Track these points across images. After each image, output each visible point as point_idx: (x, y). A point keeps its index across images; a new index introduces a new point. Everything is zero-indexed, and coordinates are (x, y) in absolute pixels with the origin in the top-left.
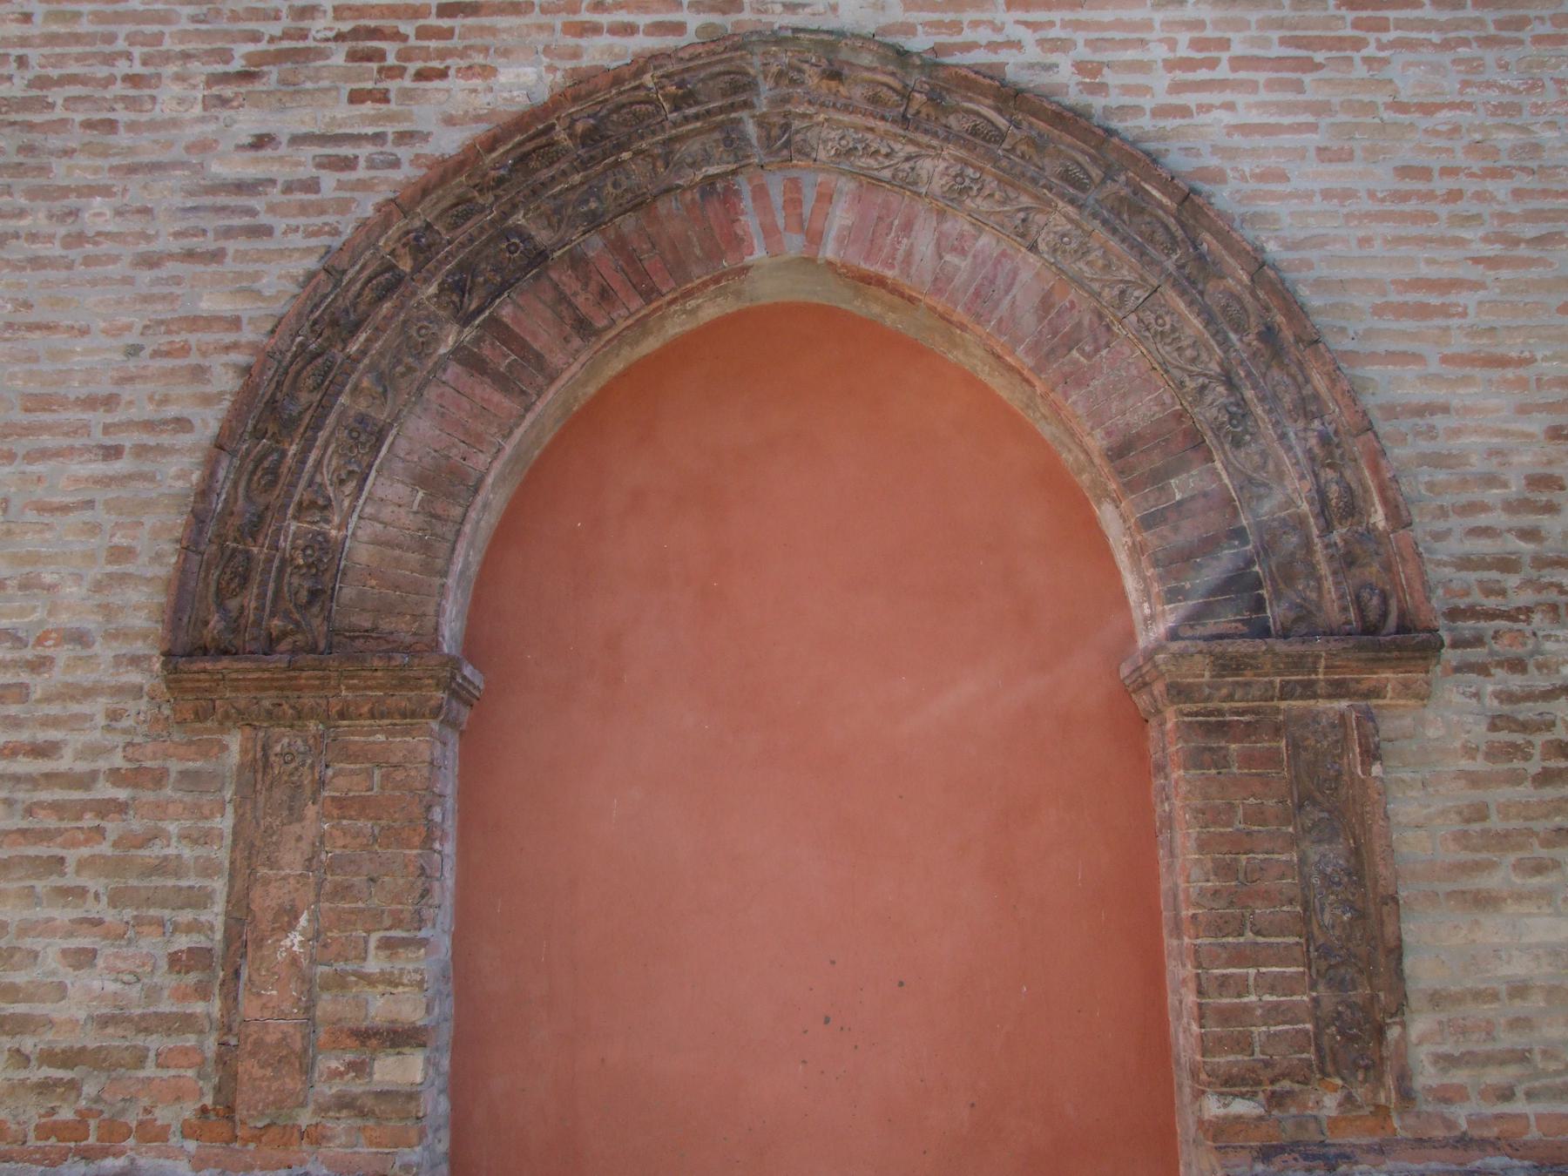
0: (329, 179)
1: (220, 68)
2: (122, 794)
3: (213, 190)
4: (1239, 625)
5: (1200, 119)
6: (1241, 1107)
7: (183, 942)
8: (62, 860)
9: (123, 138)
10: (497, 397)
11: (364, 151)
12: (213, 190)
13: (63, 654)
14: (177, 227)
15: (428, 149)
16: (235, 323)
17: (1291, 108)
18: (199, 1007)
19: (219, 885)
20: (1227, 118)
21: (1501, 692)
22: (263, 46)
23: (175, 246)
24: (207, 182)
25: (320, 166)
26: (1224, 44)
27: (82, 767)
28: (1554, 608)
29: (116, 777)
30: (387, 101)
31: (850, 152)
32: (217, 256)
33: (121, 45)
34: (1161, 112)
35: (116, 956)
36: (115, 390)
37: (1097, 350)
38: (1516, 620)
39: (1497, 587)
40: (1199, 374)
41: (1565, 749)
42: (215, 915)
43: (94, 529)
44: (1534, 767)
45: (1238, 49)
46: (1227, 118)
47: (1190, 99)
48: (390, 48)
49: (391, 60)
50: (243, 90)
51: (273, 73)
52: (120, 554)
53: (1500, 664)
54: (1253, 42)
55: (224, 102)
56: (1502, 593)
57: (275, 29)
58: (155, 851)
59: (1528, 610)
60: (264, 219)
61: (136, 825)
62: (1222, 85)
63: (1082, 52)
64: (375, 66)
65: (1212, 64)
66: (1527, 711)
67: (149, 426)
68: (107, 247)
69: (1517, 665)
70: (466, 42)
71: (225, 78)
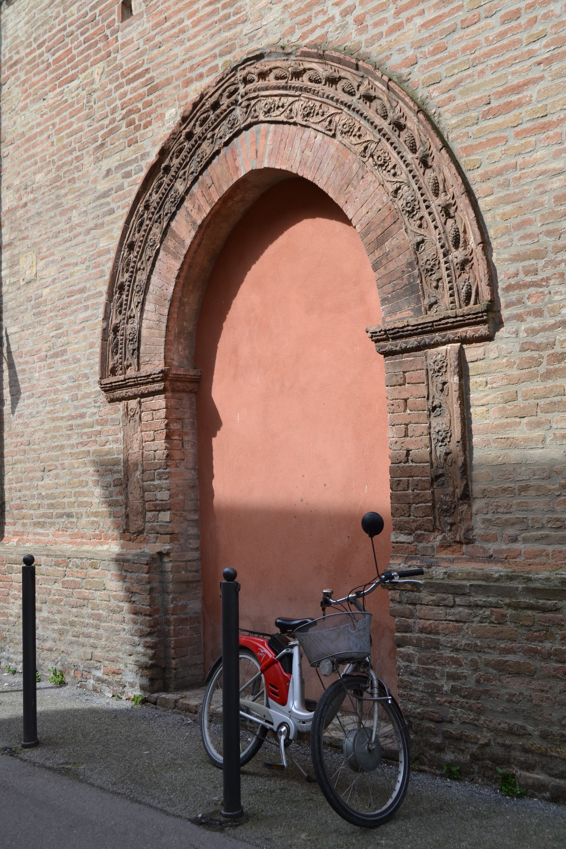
3: (98, 198)
4: (410, 312)
6: (402, 538)
12: (98, 198)
28: (562, 275)
29: (98, 423)
37: (359, 182)
38: (541, 286)
39: (532, 268)
40: (397, 182)
41: (560, 357)
44: (542, 369)
46: (419, 21)
53: (529, 314)
56: (536, 272)
57: (106, 122)
59: (548, 279)
61: (103, 438)
66: (539, 339)
69: (538, 313)
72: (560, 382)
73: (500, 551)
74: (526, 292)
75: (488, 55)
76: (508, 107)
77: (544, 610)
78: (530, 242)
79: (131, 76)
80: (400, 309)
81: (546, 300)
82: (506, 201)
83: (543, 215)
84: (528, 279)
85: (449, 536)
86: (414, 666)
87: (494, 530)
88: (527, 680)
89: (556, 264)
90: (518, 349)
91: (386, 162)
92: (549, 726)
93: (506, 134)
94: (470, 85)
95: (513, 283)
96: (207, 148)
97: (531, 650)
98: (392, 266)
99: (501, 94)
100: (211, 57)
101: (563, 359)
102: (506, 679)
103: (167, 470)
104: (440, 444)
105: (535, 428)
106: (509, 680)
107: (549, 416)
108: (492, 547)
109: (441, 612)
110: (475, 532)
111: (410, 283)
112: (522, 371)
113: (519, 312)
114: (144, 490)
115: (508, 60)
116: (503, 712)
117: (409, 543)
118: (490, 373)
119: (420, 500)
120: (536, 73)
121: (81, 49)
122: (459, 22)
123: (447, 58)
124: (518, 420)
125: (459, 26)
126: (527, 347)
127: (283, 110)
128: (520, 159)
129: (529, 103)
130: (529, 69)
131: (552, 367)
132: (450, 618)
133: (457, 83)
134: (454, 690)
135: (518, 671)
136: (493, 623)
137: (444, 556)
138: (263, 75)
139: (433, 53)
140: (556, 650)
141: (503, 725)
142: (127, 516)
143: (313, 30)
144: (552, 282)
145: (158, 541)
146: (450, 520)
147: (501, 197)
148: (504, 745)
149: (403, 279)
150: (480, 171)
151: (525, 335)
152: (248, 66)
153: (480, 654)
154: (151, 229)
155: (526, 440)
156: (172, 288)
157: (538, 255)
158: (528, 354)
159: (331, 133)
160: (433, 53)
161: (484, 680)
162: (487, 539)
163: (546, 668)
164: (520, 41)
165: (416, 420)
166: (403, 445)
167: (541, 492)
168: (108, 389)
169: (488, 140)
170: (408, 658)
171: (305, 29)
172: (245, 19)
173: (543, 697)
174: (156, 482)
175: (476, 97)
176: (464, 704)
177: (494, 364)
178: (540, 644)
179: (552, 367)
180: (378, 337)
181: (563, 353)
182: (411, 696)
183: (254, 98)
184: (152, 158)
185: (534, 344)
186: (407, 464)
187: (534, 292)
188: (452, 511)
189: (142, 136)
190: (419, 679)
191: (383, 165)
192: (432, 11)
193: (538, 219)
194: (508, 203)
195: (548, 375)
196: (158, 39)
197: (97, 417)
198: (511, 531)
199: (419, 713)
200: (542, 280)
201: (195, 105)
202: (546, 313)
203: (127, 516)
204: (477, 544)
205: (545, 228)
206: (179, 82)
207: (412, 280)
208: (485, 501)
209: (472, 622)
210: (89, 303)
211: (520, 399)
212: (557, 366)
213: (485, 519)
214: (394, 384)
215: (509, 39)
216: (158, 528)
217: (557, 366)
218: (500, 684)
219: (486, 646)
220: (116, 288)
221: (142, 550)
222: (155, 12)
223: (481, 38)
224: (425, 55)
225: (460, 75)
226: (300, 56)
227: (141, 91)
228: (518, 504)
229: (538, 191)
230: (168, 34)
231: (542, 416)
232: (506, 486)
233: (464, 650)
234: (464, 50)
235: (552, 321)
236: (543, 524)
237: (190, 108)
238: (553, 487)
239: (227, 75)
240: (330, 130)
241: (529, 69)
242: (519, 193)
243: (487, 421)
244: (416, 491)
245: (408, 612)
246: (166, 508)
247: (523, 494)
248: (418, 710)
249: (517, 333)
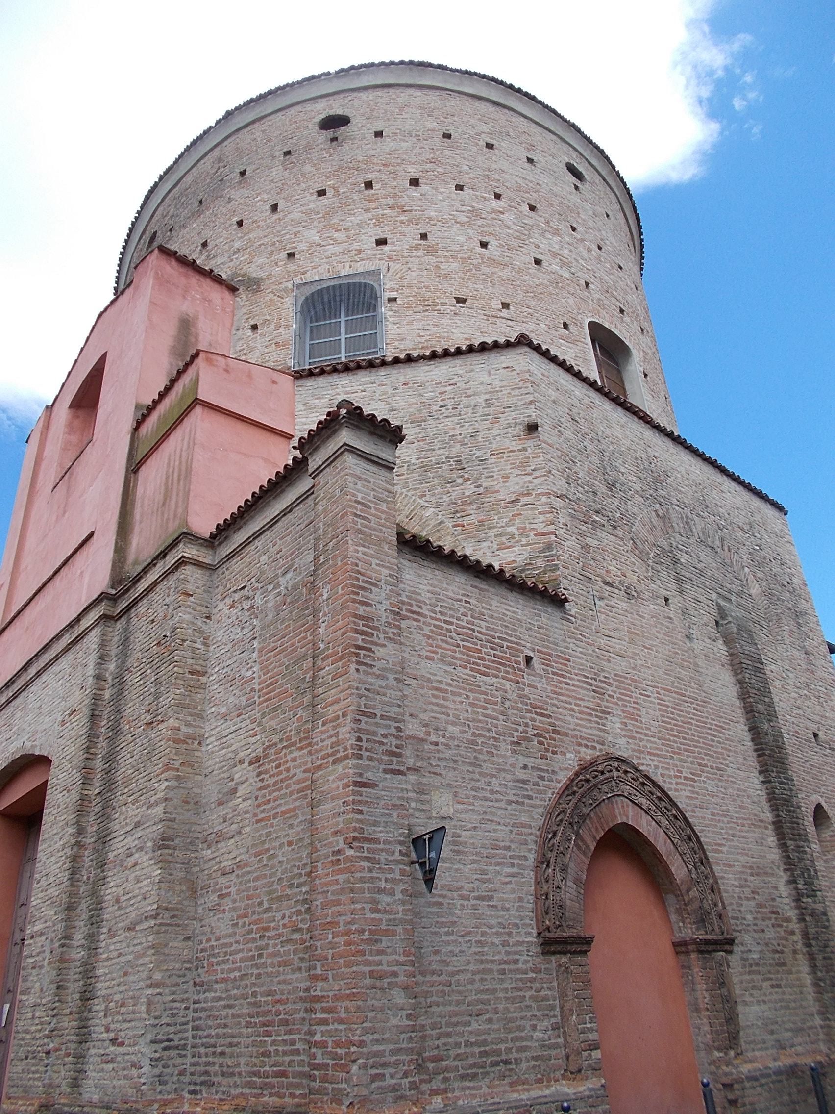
3: (519, 781)
12: (519, 781)
23: (514, 799)
27: (524, 967)
42: (557, 1012)
43: (513, 891)
58: (543, 993)
60: (530, 793)
68: (499, 796)
71: (513, 743)
142: (568, 1057)
196: (555, 702)
203: (568, 1057)
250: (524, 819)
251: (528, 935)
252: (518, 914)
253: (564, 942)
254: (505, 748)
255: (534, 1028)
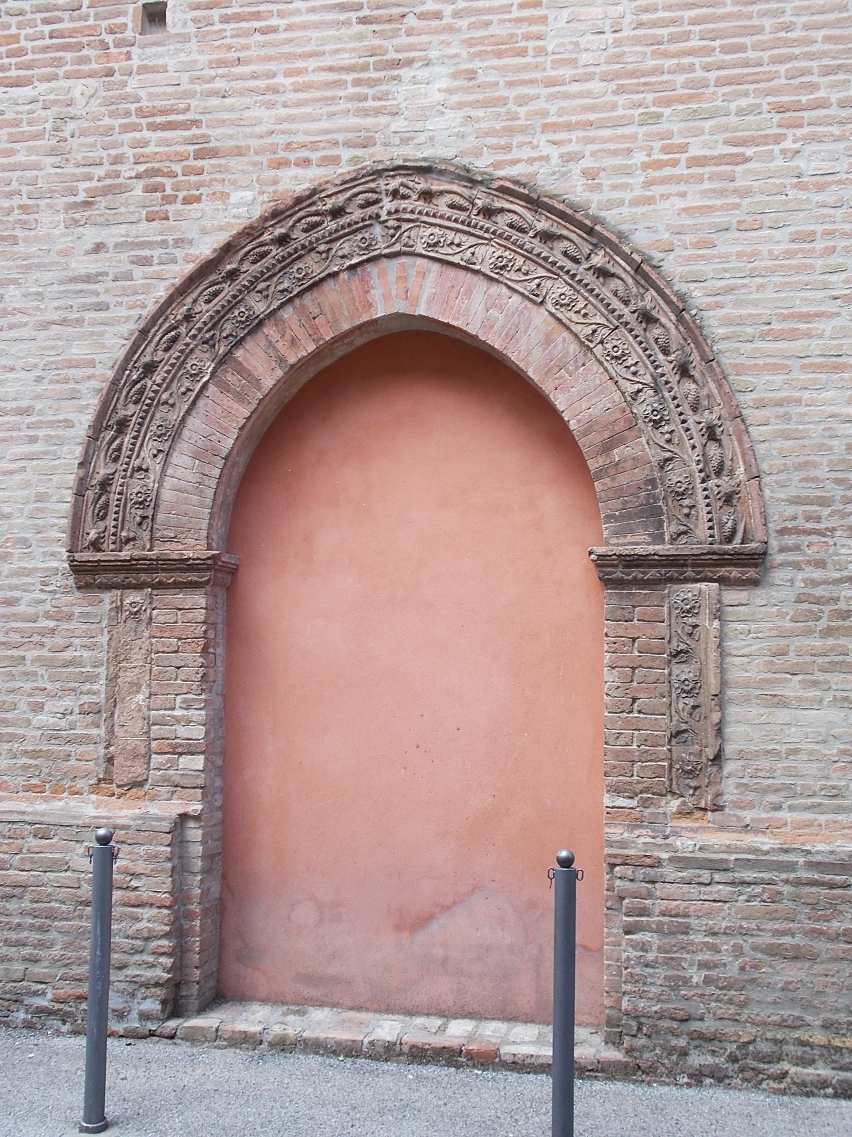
0: (138, 271)
1: (72, 199)
2: (52, 624)
3: (73, 280)
5: (660, 205)
6: (621, 802)
7: (85, 699)
8: (24, 658)
9: (21, 248)
10: (236, 406)
11: (156, 253)
12: (73, 280)
13: (17, 552)
14: (56, 304)
15: (194, 251)
16: (92, 364)
17: (722, 193)
18: (94, 731)
19: (102, 670)
20: (680, 203)
21: (808, 579)
22: (94, 184)
23: (56, 317)
24: (71, 275)
25: (132, 262)
26: (684, 148)
27: (31, 610)
30: (167, 218)
31: (436, 245)
32: (80, 322)
33: (14, 185)
34: (636, 202)
35: (54, 705)
36: (32, 403)
37: (577, 368)
38: (824, 536)
39: (815, 515)
40: (638, 382)
41: (845, 615)
42: (100, 686)
43: (27, 485)
44: (823, 624)
45: (694, 151)
46: (680, 203)
47: (656, 190)
48: (168, 183)
49: (169, 191)
50: (85, 214)
51: (102, 202)
52: (41, 498)
53: (809, 562)
54: (705, 145)
55: (76, 223)
56: (818, 520)
57: (100, 172)
58: (68, 654)
59: (834, 529)
60: (103, 298)
61: (60, 641)
62: (679, 180)
63: (588, 163)
64: (159, 195)
65: (674, 163)
66: (819, 592)
67: (51, 424)
68: (19, 318)
69: (820, 564)
70: (212, 176)
71: (75, 206)
72: (842, 641)
73: (761, 820)
74: (805, 539)
75: (773, 270)
76: (793, 335)
77: (832, 886)
78: (814, 486)
79: (159, 119)
80: (632, 531)
81: (831, 551)
82: (786, 435)
83: (831, 460)
84: (810, 525)
85: (690, 802)
86: (651, 956)
87: (750, 797)
88: (807, 965)
89: (844, 516)
90: (793, 600)
91: (624, 356)
92: (834, 1014)
93: (789, 363)
94: (744, 297)
95: (790, 526)
96: (313, 266)
97: (814, 931)
98: (622, 479)
99: (785, 318)
100: (328, 142)
101: (849, 617)
102: (780, 965)
103: (202, 697)
104: (684, 695)
105: (810, 687)
106: (784, 965)
107: (828, 676)
108: (748, 816)
109: (692, 891)
110: (725, 798)
111: (648, 503)
112: (797, 624)
113: (796, 559)
114: (150, 723)
115: (796, 282)
116: (775, 1003)
117: (632, 808)
118: (754, 621)
119: (649, 758)
120: (831, 307)
121: (40, 43)
122: (734, 221)
123: (715, 256)
124: (789, 676)
125: (735, 226)
126: (804, 598)
127: (458, 250)
128: (806, 395)
129: (821, 336)
130: (821, 301)
131: (834, 624)
132: (706, 897)
133: (730, 290)
134: (707, 981)
135: (796, 956)
136: (764, 901)
137: (684, 825)
138: (427, 196)
139: (697, 245)
140: (845, 930)
141: (773, 1018)
142: (110, 760)
143: (514, 162)
144: (838, 533)
145: (175, 796)
146: (693, 783)
147: (779, 430)
148: (775, 1041)
149: (638, 497)
150: (753, 395)
151: (803, 585)
152: (400, 175)
153: (745, 938)
154: (192, 350)
155: (800, 699)
156: (231, 442)
157: (823, 502)
158: (805, 606)
159: (539, 300)
160: (697, 245)
161: (751, 968)
162: (740, 805)
163: (832, 950)
164: (812, 267)
165: (650, 664)
166: (628, 691)
167: (813, 756)
168: (79, 569)
169: (766, 364)
170: (644, 947)
171: (500, 157)
172: (395, 111)
173: (828, 982)
174: (178, 713)
175: (754, 312)
176: (721, 996)
177: (759, 613)
178: (826, 924)
179: (834, 624)
180: (602, 562)
181: (848, 611)
182: (644, 991)
183: (409, 221)
184: (206, 249)
185: (814, 597)
186: (631, 715)
187: (816, 541)
188: (697, 773)
189: (178, 213)
190: (657, 970)
191: (620, 359)
192: (698, 196)
193: (825, 464)
194: (786, 439)
195: (828, 632)
196: (219, 85)
197: (48, 607)
198: (773, 798)
199: (656, 1012)
200: (827, 529)
201: (298, 201)
202: (829, 566)
203: (110, 760)
204: (727, 809)
205: (833, 475)
206: (264, 159)
207: (652, 501)
208: (742, 762)
209: (736, 901)
210: (41, 433)
211: (792, 654)
212: (841, 623)
213: (740, 784)
214: (618, 618)
215: (799, 261)
216: (177, 779)
217: (841, 623)
218: (771, 970)
219: (755, 927)
220: (109, 425)
221: (143, 810)
222: (217, 43)
223: (764, 249)
224: (685, 244)
225: (732, 281)
226: (495, 190)
227: (180, 148)
228: (784, 768)
229: (826, 434)
230: (240, 84)
231: (821, 677)
232: (770, 747)
233: (724, 933)
234: (740, 255)
235: (837, 575)
236: (815, 792)
237: (289, 202)
238: (830, 752)
239: (363, 176)
240: (537, 295)
241: (821, 301)
242: (802, 430)
243: (748, 674)
244: (643, 747)
245: (644, 892)
246: (198, 750)
247: (791, 757)
248: (654, 1009)
249: (792, 581)
250: (78, 350)
251: (50, 555)
252: (31, 522)
253: (128, 566)
254: (51, 221)
255: (38, 708)
